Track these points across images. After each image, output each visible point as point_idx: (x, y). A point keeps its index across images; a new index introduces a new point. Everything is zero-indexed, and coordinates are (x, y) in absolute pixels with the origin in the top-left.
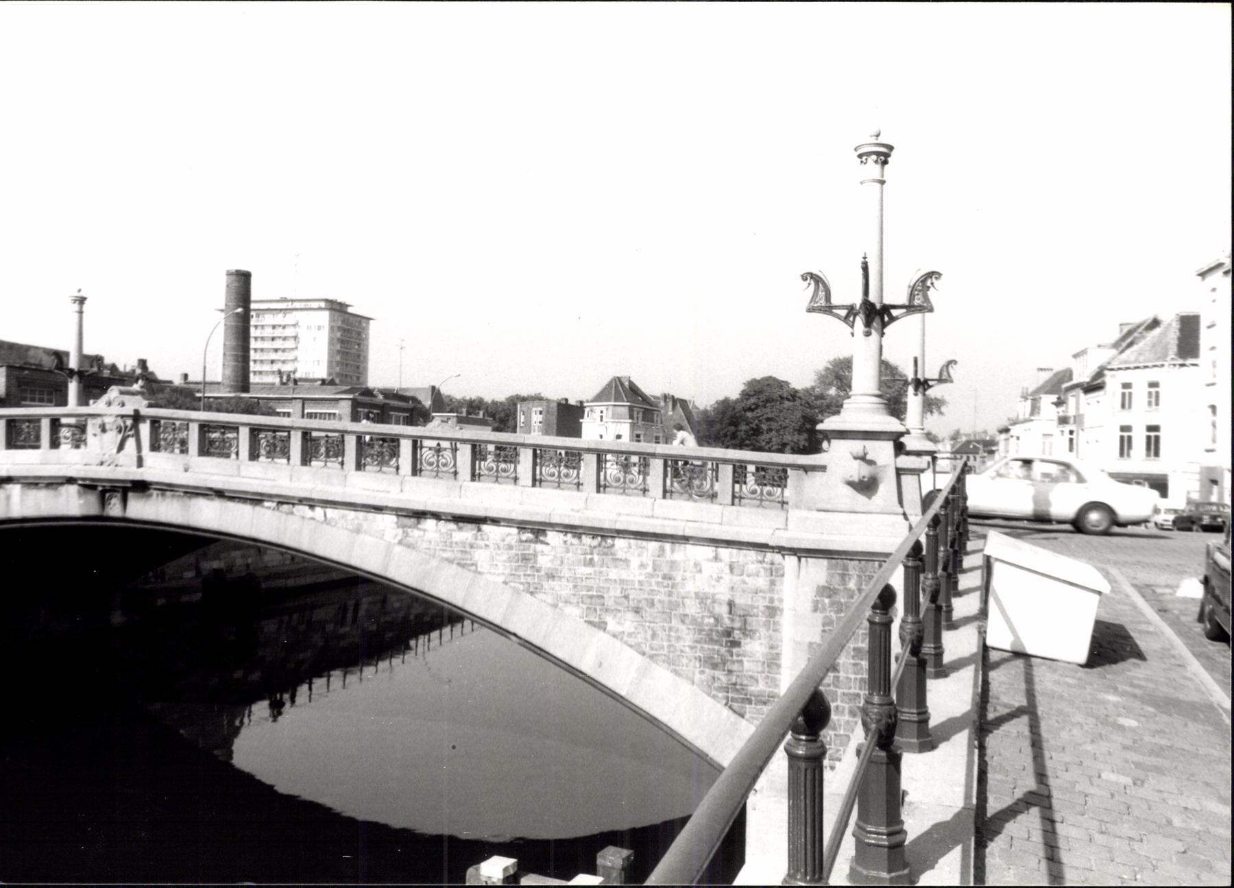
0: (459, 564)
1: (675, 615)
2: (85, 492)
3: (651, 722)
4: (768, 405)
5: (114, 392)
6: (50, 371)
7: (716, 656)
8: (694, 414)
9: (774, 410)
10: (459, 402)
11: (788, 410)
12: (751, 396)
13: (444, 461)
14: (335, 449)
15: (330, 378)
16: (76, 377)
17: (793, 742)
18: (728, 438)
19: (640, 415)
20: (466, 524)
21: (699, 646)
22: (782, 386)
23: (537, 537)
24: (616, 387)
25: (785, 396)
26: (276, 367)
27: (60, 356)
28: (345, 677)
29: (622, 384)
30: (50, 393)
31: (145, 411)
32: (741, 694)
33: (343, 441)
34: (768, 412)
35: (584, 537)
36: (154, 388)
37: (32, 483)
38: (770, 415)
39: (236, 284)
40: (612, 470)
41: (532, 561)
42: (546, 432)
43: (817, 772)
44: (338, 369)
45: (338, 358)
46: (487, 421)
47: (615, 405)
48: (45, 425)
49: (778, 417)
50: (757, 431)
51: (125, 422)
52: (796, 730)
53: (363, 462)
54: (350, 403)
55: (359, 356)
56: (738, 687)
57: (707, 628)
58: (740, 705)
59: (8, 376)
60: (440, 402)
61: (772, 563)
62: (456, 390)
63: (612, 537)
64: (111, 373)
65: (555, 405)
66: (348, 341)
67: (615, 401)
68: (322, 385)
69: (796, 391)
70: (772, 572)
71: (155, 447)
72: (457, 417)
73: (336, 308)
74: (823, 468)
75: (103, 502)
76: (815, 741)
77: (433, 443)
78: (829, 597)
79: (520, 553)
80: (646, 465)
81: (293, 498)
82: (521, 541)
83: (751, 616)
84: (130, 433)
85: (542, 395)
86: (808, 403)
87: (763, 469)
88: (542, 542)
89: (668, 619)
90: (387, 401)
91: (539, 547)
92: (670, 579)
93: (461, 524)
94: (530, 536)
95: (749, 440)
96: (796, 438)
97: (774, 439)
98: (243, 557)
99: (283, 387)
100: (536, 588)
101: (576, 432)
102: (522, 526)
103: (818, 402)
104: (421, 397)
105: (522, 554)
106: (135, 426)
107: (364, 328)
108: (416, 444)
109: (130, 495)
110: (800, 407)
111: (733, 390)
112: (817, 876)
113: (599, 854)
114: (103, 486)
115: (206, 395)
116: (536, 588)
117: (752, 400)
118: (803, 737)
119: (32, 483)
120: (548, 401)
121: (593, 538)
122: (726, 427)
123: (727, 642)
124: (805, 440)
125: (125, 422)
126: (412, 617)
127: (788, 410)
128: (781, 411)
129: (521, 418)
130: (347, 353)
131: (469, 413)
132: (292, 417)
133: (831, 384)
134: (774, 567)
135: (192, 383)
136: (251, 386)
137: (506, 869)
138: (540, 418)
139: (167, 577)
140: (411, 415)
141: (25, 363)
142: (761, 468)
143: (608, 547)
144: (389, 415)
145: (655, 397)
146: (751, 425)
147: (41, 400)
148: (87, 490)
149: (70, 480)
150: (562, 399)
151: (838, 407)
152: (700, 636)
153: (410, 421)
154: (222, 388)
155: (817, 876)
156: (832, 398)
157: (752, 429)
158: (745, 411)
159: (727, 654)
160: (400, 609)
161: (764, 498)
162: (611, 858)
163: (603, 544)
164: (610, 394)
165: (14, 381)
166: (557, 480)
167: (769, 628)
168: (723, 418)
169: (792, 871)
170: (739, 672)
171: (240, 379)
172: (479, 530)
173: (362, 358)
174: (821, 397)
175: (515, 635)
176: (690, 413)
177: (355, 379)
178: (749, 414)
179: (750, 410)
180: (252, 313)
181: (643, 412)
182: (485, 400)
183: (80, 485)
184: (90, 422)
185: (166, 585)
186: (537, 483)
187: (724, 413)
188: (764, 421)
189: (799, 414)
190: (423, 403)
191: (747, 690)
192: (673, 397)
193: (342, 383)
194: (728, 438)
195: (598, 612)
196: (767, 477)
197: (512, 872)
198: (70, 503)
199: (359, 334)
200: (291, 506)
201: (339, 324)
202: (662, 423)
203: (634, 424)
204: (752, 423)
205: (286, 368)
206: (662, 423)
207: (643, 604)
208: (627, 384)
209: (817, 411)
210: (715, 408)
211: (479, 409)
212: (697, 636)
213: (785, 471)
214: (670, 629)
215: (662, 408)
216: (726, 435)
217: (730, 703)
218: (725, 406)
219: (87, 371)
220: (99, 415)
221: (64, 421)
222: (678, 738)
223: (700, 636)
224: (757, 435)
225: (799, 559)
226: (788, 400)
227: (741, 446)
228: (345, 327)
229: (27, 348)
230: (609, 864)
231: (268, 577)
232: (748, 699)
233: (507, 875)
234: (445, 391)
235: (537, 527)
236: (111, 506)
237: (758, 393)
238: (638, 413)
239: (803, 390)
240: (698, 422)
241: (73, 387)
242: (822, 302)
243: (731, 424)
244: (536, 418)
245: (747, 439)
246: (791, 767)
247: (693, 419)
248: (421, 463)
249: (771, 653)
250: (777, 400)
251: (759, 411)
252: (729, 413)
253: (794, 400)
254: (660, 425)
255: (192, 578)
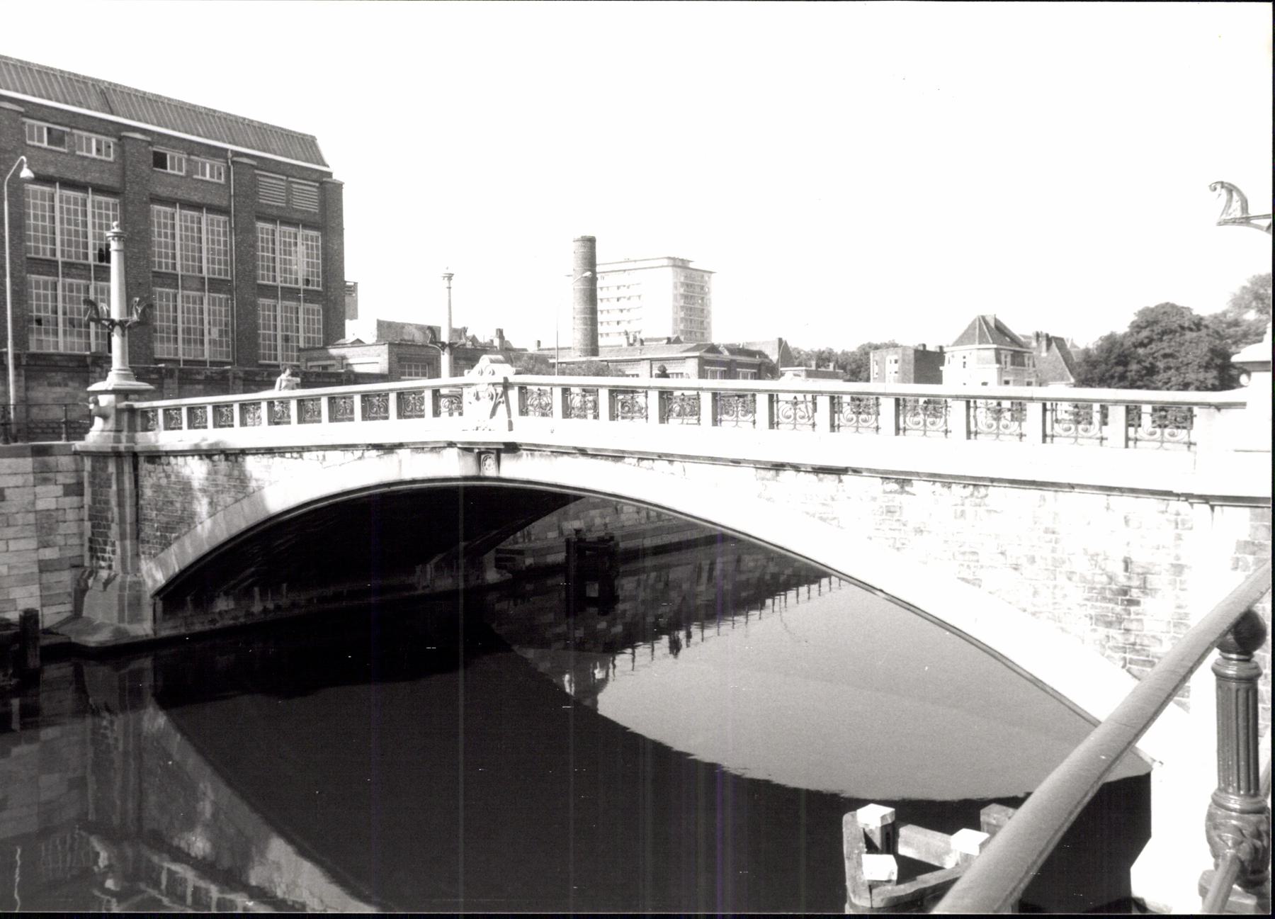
0: (821, 518)
1: (1060, 572)
2: (463, 455)
3: (1035, 684)
4: (1165, 338)
5: (485, 360)
6: (424, 346)
7: (1110, 614)
8: (1073, 355)
9: (1173, 344)
10: (807, 354)
11: (1191, 342)
12: (1142, 328)
13: (802, 414)
14: (692, 408)
15: (676, 336)
16: (447, 350)
17: (1221, 661)
18: (1116, 379)
19: (1009, 359)
20: (826, 475)
21: (1089, 604)
22: (1183, 313)
23: (902, 487)
24: (980, 324)
25: (1186, 325)
26: (622, 327)
27: (434, 331)
28: (702, 631)
29: (986, 323)
30: (424, 367)
31: (513, 379)
32: (1142, 655)
33: (699, 399)
34: (1165, 346)
35: (954, 486)
36: (510, 354)
37: (419, 447)
38: (1168, 351)
39: (582, 250)
40: (983, 417)
41: (897, 514)
42: (904, 380)
43: (1250, 694)
44: (682, 327)
45: (682, 314)
46: (837, 373)
47: (979, 349)
48: (428, 395)
49: (1178, 351)
50: (1152, 371)
51: (496, 390)
52: (1224, 648)
53: (719, 417)
54: (696, 361)
55: (702, 310)
56: (1138, 647)
57: (1098, 586)
58: (1140, 668)
59: (390, 353)
60: (788, 356)
61: (1178, 514)
62: (804, 343)
63: (985, 486)
64: (473, 344)
65: (911, 353)
66: (692, 296)
67: (980, 343)
68: (667, 343)
69: (1201, 319)
70: (1177, 524)
71: (523, 411)
72: (806, 370)
73: (680, 265)
74: (1243, 405)
75: (479, 462)
76: (1248, 661)
77: (790, 397)
78: (1254, 553)
79: (884, 505)
80: (1022, 409)
81: (653, 454)
82: (885, 492)
83: (1152, 574)
84: (501, 400)
85: (897, 342)
86: (1218, 333)
87: (1162, 409)
88: (908, 493)
89: (1052, 577)
90: (734, 357)
91: (904, 498)
92: (1054, 533)
93: (821, 476)
94: (895, 487)
95: (1141, 381)
96: (1201, 376)
97: (1173, 379)
98: (603, 517)
99: (631, 348)
100: (903, 544)
101: (937, 379)
102: (886, 476)
103: (1232, 331)
104: (767, 352)
105: (887, 506)
106: (505, 393)
107: (706, 282)
108: (772, 399)
109: (503, 455)
110: (1207, 338)
111: (1121, 324)
112: (1252, 792)
113: (982, 811)
114: (479, 449)
115: (560, 361)
116: (903, 544)
117: (1145, 333)
118: (1234, 656)
119: (419, 447)
120: (905, 348)
121: (964, 487)
122: (1112, 367)
123: (1122, 600)
124: (1215, 377)
125: (496, 390)
126: (768, 577)
127: (1191, 342)
128: (1182, 344)
129: (874, 369)
130: (691, 309)
131: (818, 366)
132: (643, 377)
133: (1248, 307)
134: (1179, 518)
135: (545, 349)
136: (600, 349)
137: (883, 818)
138: (896, 367)
139: (533, 538)
140: (759, 370)
141: (401, 340)
142: (1161, 410)
143: (982, 498)
144: (736, 372)
145: (1025, 337)
146: (1143, 364)
147: (417, 374)
148: (465, 453)
149: (451, 445)
150: (919, 345)
151: (1258, 335)
152: (1091, 595)
153: (758, 376)
154: (572, 353)
155: (1252, 792)
156: (1250, 325)
157: (1145, 368)
158: (1136, 347)
159: (1123, 612)
160: (756, 567)
161: (1165, 440)
162: (995, 816)
163: (976, 493)
164: (974, 335)
165: (395, 358)
166: (923, 428)
167: (1176, 588)
168: (1109, 357)
169: (1223, 785)
170: (1140, 631)
171: (588, 342)
172: (840, 481)
173: (705, 312)
174: (1236, 323)
175: (881, 591)
176: (1069, 353)
177: (698, 335)
178: (1141, 351)
179: (1142, 345)
180: (598, 276)
181: (1012, 355)
182: (835, 351)
183: (459, 448)
184: (465, 390)
185: (532, 545)
186: (901, 432)
187: (1110, 351)
188: (1160, 358)
189: (1204, 347)
190: (770, 357)
191: (1149, 651)
192: (1047, 336)
193: (688, 340)
194: (1116, 379)
195: (972, 568)
196: (1169, 417)
197: (890, 821)
198: (452, 467)
199: (702, 288)
200: (651, 461)
201: (682, 279)
202: (1034, 366)
203: (1002, 369)
204: (1145, 361)
205: (631, 328)
206: (1034, 366)
207: (1023, 561)
208: (992, 324)
209: (1229, 341)
210: (1098, 346)
211: (829, 362)
212: (1087, 595)
213: (1190, 410)
214: (1055, 587)
215: (1034, 348)
216: (1112, 377)
217: (1128, 666)
218: (1111, 343)
219: (456, 343)
220: (473, 384)
221: (443, 391)
222: (1067, 703)
223: (1091, 595)
224: (1152, 376)
225: (1212, 507)
226: (1191, 330)
227: (1132, 386)
228: (689, 282)
229: (403, 326)
230: (994, 822)
231: (625, 537)
232: (1150, 661)
233: (885, 823)
234: (792, 344)
235: (904, 477)
236: (487, 466)
237: (1150, 324)
238: (1006, 357)
239: (1211, 316)
240: (1077, 363)
241: (445, 359)
242: (1238, 214)
243: (1117, 364)
244: (891, 368)
245: (1138, 380)
246: (1219, 687)
247: (1073, 360)
248: (778, 417)
249: (1179, 614)
250: (1175, 332)
251: (1153, 345)
252: (1116, 351)
253: (1199, 330)
254: (1032, 369)
255: (555, 538)
